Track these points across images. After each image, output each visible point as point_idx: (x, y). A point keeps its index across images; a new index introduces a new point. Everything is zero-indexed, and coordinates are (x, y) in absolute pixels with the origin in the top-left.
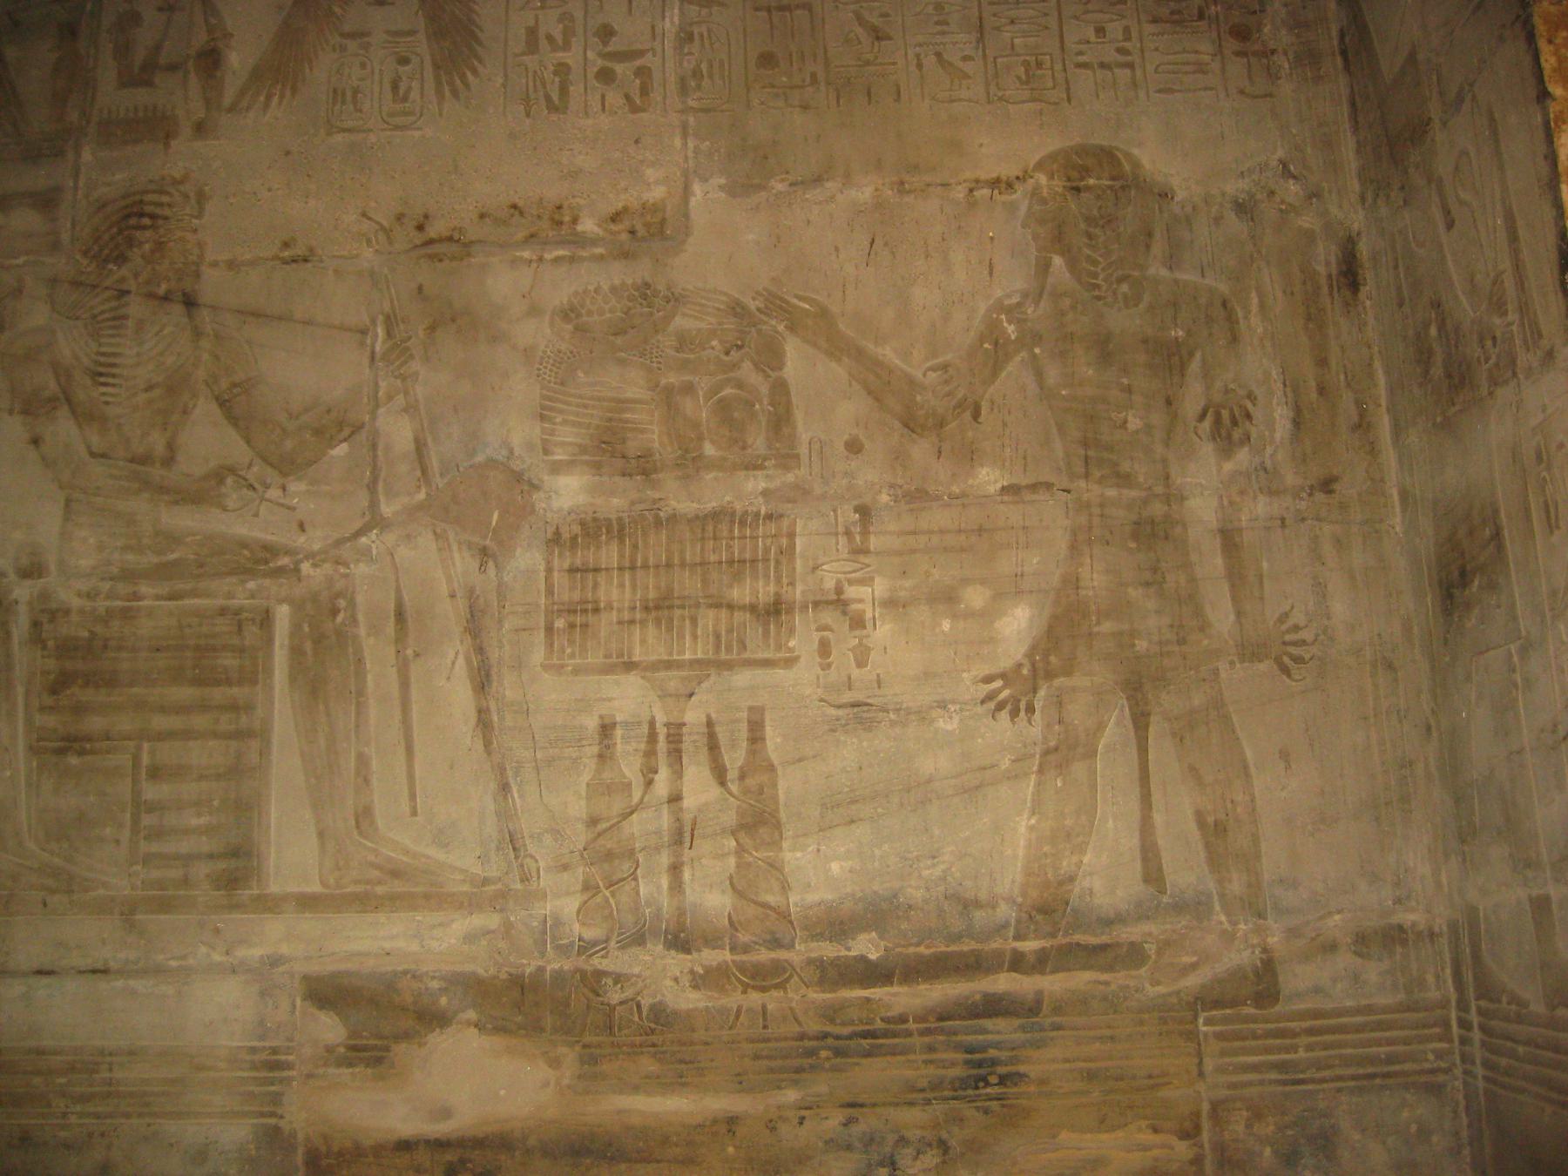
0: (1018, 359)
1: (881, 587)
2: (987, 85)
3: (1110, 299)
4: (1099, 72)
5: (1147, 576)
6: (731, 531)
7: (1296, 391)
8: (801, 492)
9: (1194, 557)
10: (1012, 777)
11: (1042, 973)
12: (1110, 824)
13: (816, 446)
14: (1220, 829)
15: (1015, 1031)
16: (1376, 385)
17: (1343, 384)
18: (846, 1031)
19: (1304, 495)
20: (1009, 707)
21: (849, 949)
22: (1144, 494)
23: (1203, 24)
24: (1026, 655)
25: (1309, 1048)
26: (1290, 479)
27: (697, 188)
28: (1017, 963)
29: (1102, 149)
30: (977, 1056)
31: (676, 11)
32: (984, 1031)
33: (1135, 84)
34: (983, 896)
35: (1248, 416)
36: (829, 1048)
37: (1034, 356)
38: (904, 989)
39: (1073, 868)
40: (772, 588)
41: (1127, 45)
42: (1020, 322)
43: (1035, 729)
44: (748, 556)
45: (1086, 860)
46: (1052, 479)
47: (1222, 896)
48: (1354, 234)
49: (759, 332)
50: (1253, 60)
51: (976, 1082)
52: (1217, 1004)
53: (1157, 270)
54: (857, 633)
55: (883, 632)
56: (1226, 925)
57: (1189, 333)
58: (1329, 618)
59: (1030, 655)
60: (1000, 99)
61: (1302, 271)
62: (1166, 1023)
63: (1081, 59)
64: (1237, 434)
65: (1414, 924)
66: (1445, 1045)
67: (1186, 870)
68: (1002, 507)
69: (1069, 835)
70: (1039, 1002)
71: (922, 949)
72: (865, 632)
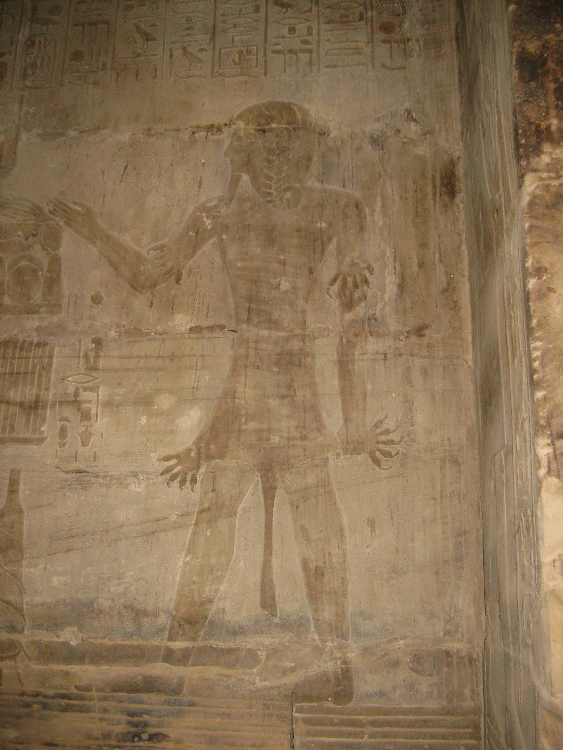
0: (211, 242)
1: (103, 393)
2: (213, 66)
3: (278, 203)
4: (287, 56)
5: (284, 391)
6: (14, 353)
7: (403, 265)
8: (61, 329)
9: (318, 380)
10: (177, 526)
11: (186, 665)
12: (242, 564)
13: (73, 299)
14: (319, 573)
15: (163, 704)
16: (462, 262)
17: (437, 260)
18: (51, 692)
19: (402, 337)
20: (179, 478)
21: (58, 637)
22: (286, 334)
23: (363, 23)
24: (194, 443)
25: (372, 735)
26: (393, 326)
27: (24, 136)
28: (169, 656)
29: (283, 104)
30: (135, 719)
31: (27, 28)
32: (141, 702)
33: (311, 63)
34: (150, 608)
35: (366, 282)
36: (39, 703)
37: (222, 240)
38: (91, 668)
39: (212, 593)
40: (34, 391)
41: (309, 38)
42: (215, 218)
43: (194, 495)
44: (22, 370)
45: (222, 588)
46: (223, 322)
47: (317, 620)
48: (455, 159)
49: (48, 226)
50: (393, 44)
51: (134, 737)
52: (307, 698)
53: (312, 183)
54: (85, 423)
55: (101, 423)
56: (318, 642)
57: (330, 225)
58: (412, 426)
59: (197, 443)
60: (220, 75)
61: (414, 183)
62: (268, 709)
63: (279, 48)
64: (357, 294)
65: (458, 651)
66: (474, 742)
67: (292, 599)
68: (189, 341)
69: (211, 570)
70: (180, 685)
71: (106, 641)
72: (89, 423)
